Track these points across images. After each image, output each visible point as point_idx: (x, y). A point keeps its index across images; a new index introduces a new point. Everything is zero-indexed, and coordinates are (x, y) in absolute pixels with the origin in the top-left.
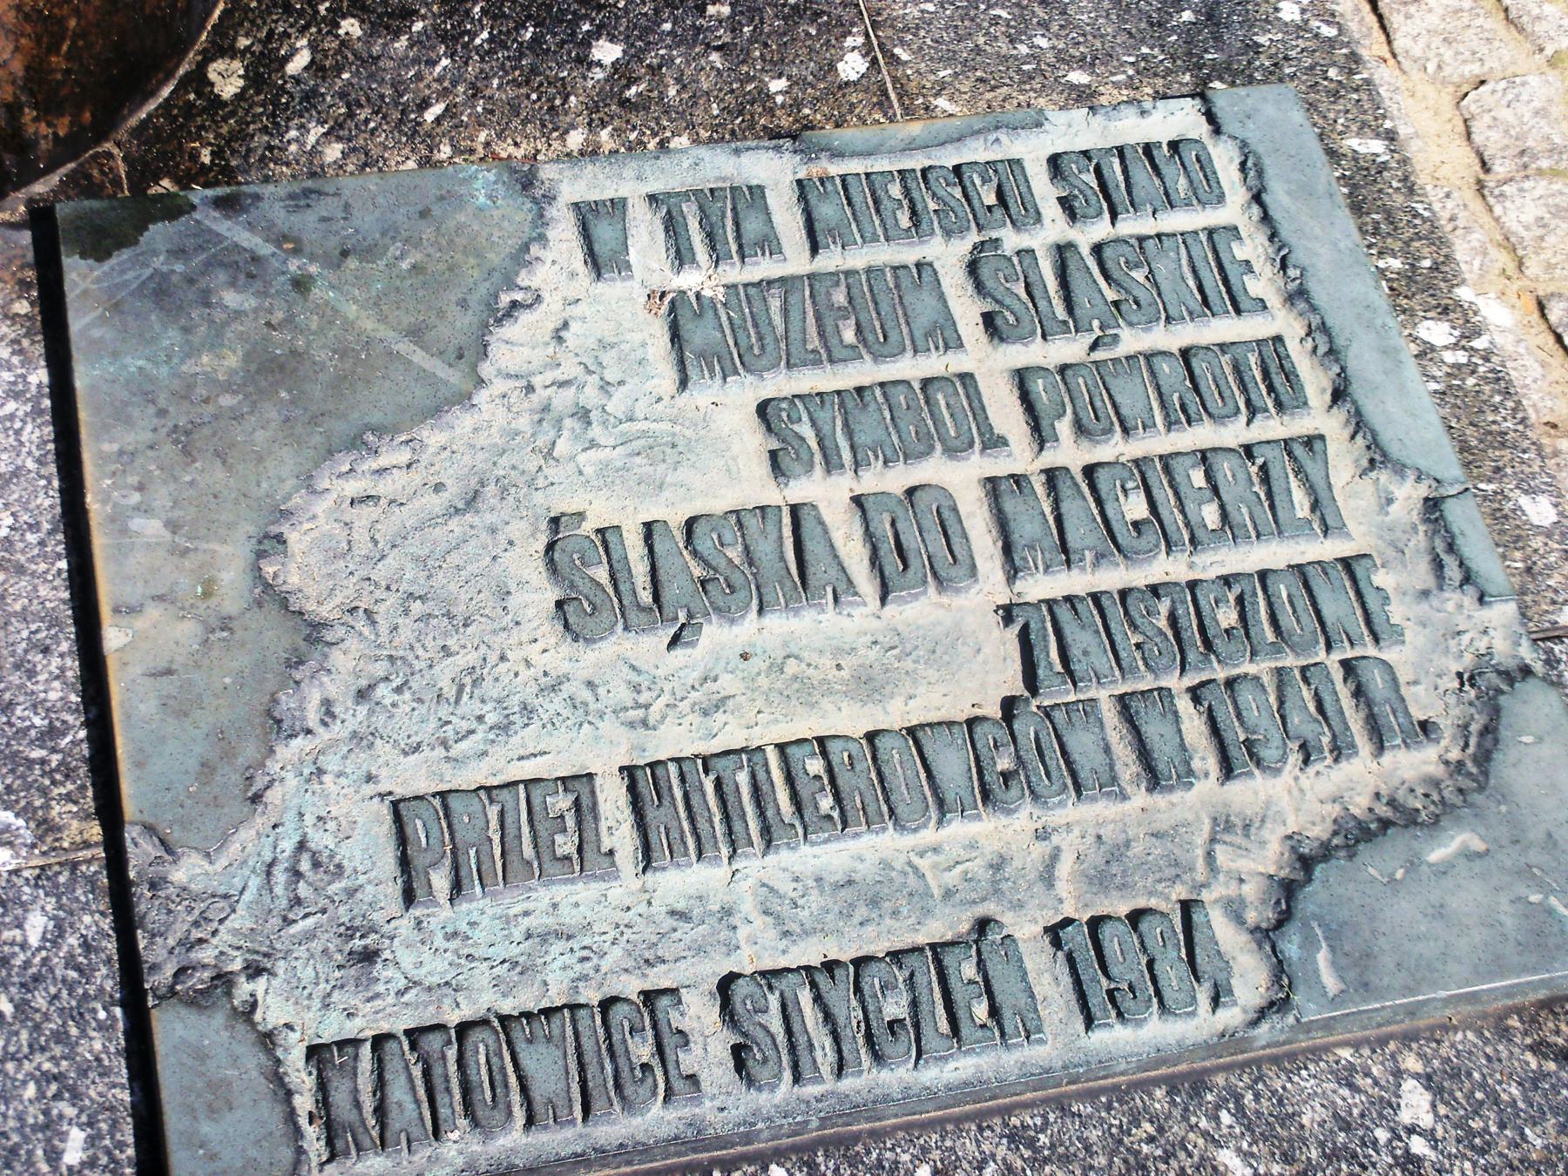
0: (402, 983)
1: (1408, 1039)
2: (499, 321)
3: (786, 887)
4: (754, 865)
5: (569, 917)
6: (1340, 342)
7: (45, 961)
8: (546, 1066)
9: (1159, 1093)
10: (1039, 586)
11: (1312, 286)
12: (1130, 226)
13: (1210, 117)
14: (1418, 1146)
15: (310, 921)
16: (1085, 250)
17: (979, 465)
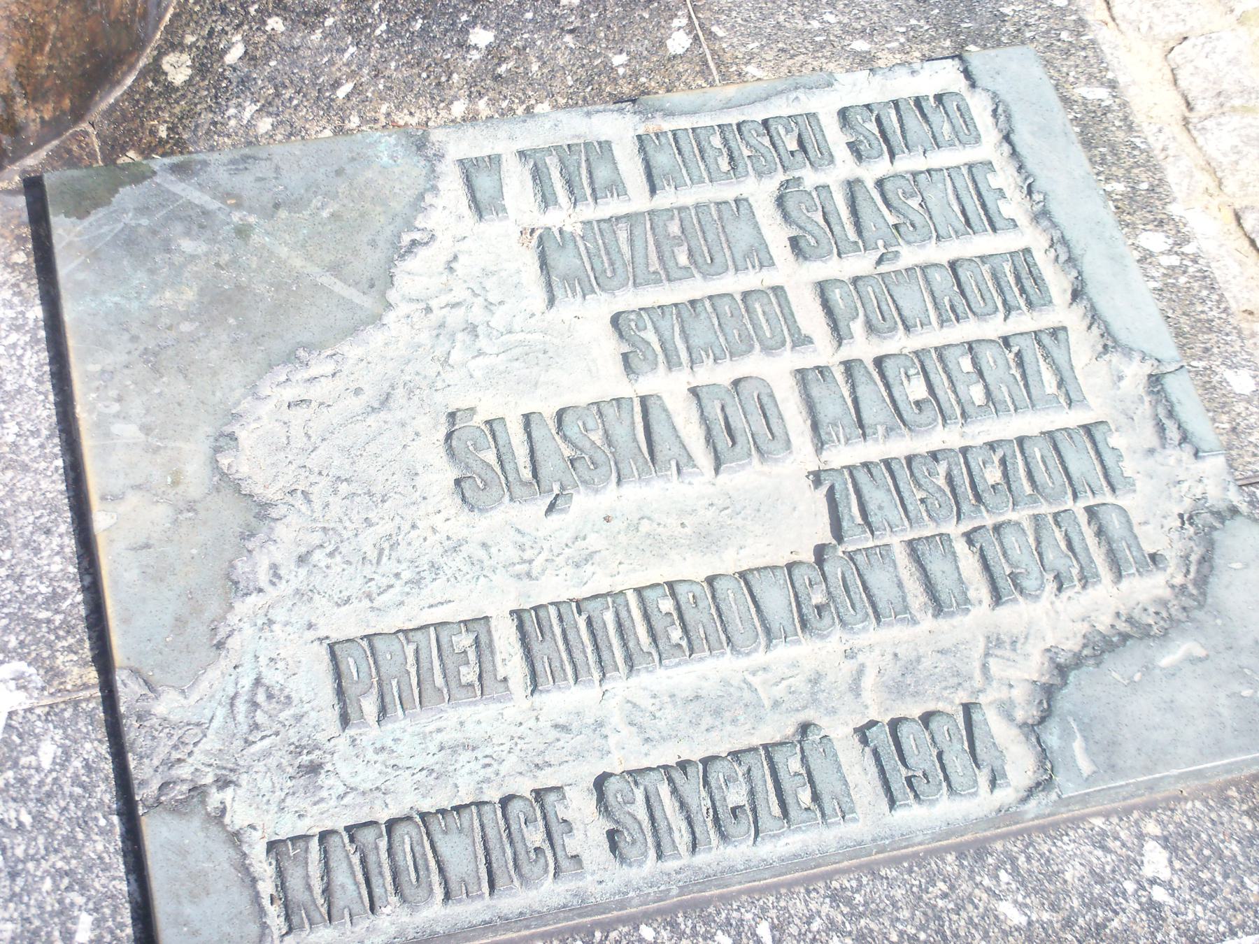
0: (342, 790)
2: (402, 257)
3: (646, 703)
4: (621, 686)
5: (473, 732)
6: (1077, 252)
7: (55, 779)
8: (459, 852)
10: (841, 455)
11: (1053, 207)
12: (907, 163)
14: (1159, 894)
15: (267, 742)
16: (870, 184)
17: (791, 359)
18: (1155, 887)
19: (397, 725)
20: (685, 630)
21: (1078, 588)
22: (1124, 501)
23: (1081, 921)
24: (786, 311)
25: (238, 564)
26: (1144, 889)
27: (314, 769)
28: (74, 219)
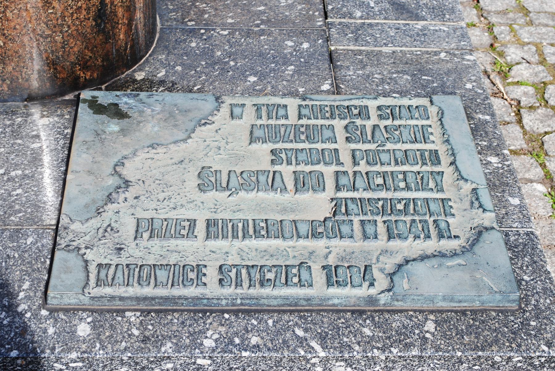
0: (128, 256)
1: (432, 312)
2: (200, 126)
3: (246, 250)
4: (237, 243)
5: (180, 248)
6: (456, 152)
7: (30, 248)
8: (162, 275)
9: (348, 314)
10: (342, 194)
11: (451, 139)
12: (397, 122)
13: (431, 101)
14: (428, 335)
15: (106, 240)
16: (382, 127)
17: (334, 168)
18: (427, 333)
19: (154, 242)
20: (267, 232)
21: (422, 241)
22: (450, 220)
23: (394, 338)
24: (337, 155)
25: (113, 194)
26: (422, 333)
27: (120, 249)
28: (92, 111)
